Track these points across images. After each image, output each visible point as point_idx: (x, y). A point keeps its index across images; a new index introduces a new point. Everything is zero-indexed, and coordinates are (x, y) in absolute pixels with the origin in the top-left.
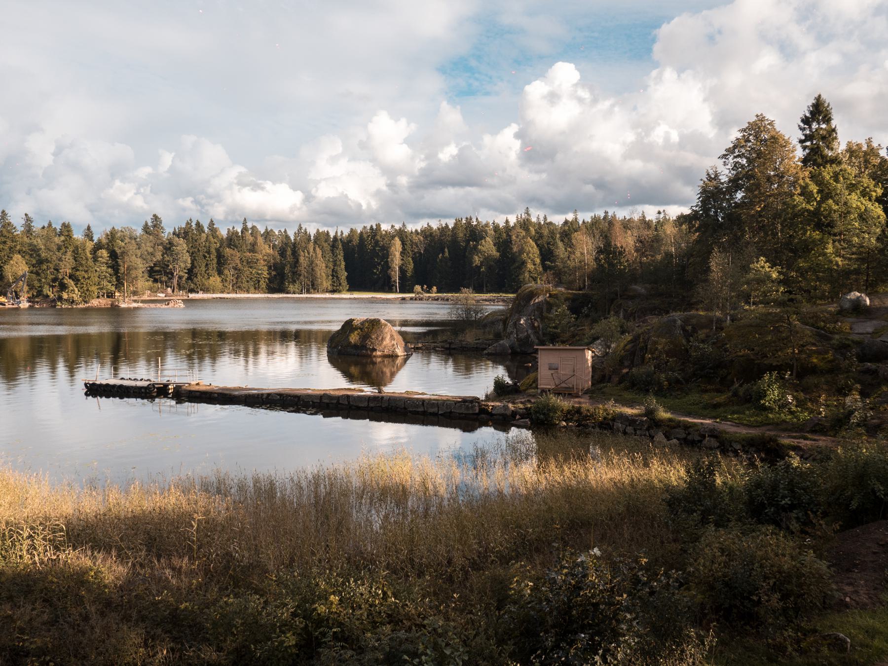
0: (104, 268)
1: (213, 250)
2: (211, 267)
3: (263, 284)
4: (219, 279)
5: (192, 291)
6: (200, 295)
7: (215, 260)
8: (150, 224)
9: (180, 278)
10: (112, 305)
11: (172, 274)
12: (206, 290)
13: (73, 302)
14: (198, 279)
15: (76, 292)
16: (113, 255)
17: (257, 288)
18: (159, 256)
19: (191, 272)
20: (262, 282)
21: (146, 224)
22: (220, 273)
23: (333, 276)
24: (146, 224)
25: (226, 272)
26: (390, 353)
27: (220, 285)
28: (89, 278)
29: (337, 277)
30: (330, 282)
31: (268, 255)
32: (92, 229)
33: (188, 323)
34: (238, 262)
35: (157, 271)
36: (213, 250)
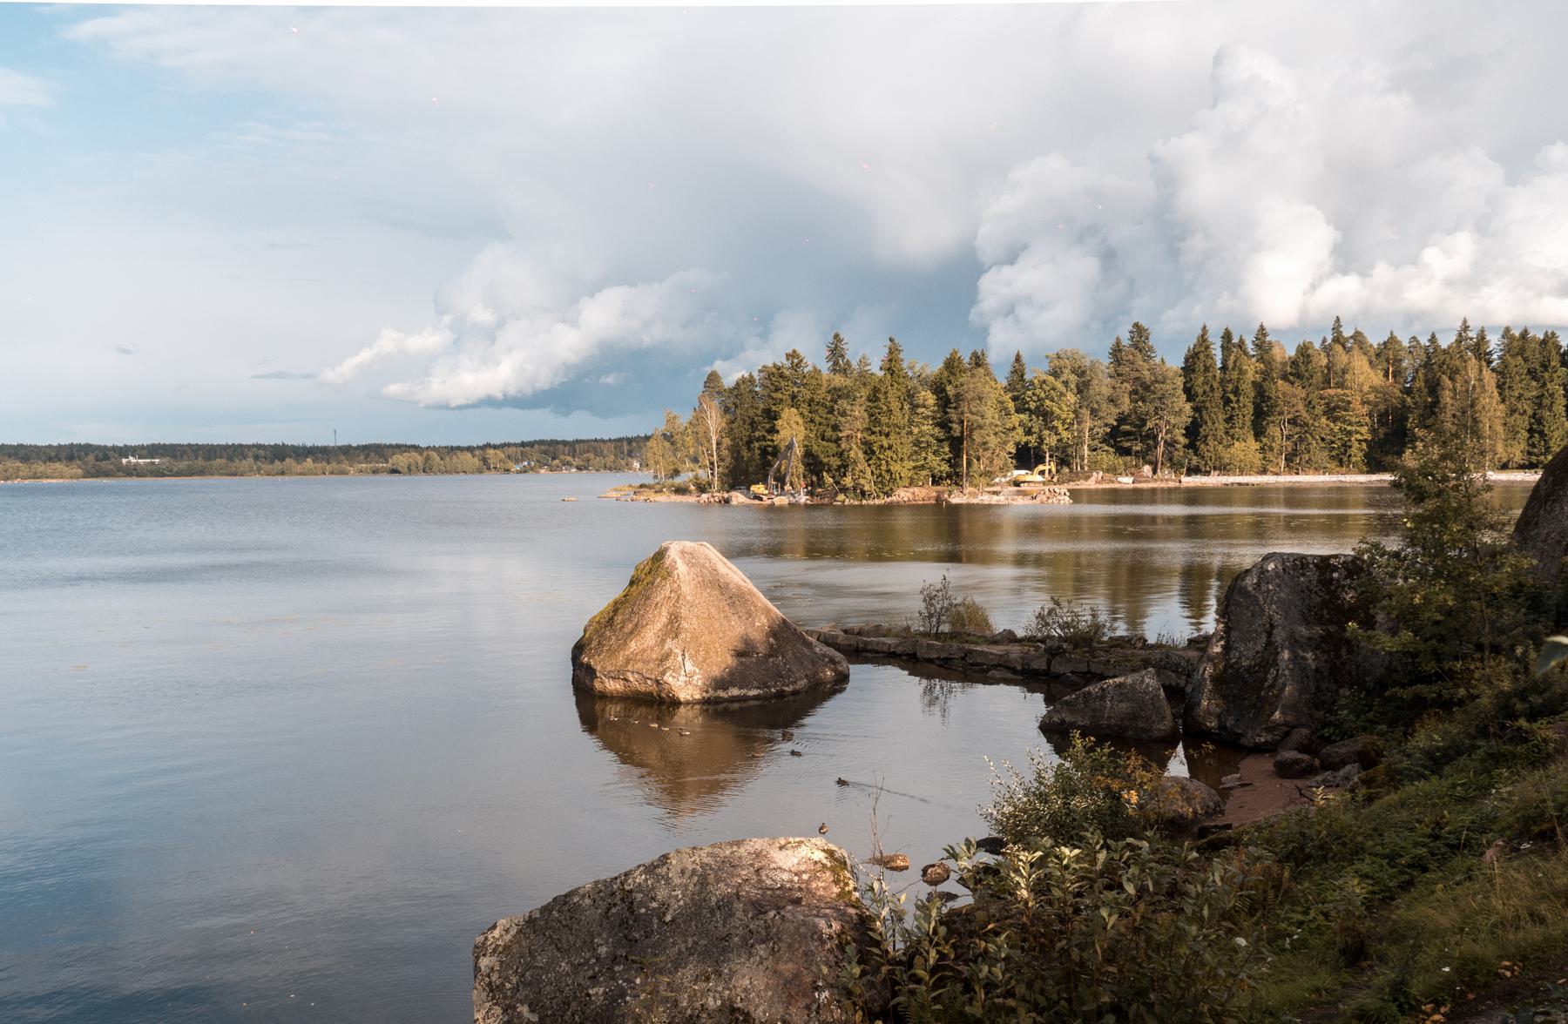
0: (927, 428)
1: (1247, 387)
2: (1239, 422)
3: (1357, 453)
4: (1255, 446)
5: (1193, 471)
6: (1214, 480)
7: (1251, 408)
8: (1126, 341)
9: (1170, 444)
10: (938, 499)
11: (1155, 437)
12: (1223, 469)
13: (863, 493)
14: (1210, 448)
15: (868, 475)
16: (944, 402)
17: (1341, 459)
18: (1126, 405)
19: (1193, 431)
20: (1353, 451)
21: (1118, 343)
22: (1259, 433)
23: (1531, 431)
24: (1118, 343)
25: (1274, 430)
26: (650, 686)
27: (1257, 459)
28: (890, 448)
29: (1542, 433)
30: (1523, 446)
31: (1374, 389)
32: (1024, 359)
33: (745, 534)
34: (1301, 407)
35: (1127, 433)
36: (1247, 387)
